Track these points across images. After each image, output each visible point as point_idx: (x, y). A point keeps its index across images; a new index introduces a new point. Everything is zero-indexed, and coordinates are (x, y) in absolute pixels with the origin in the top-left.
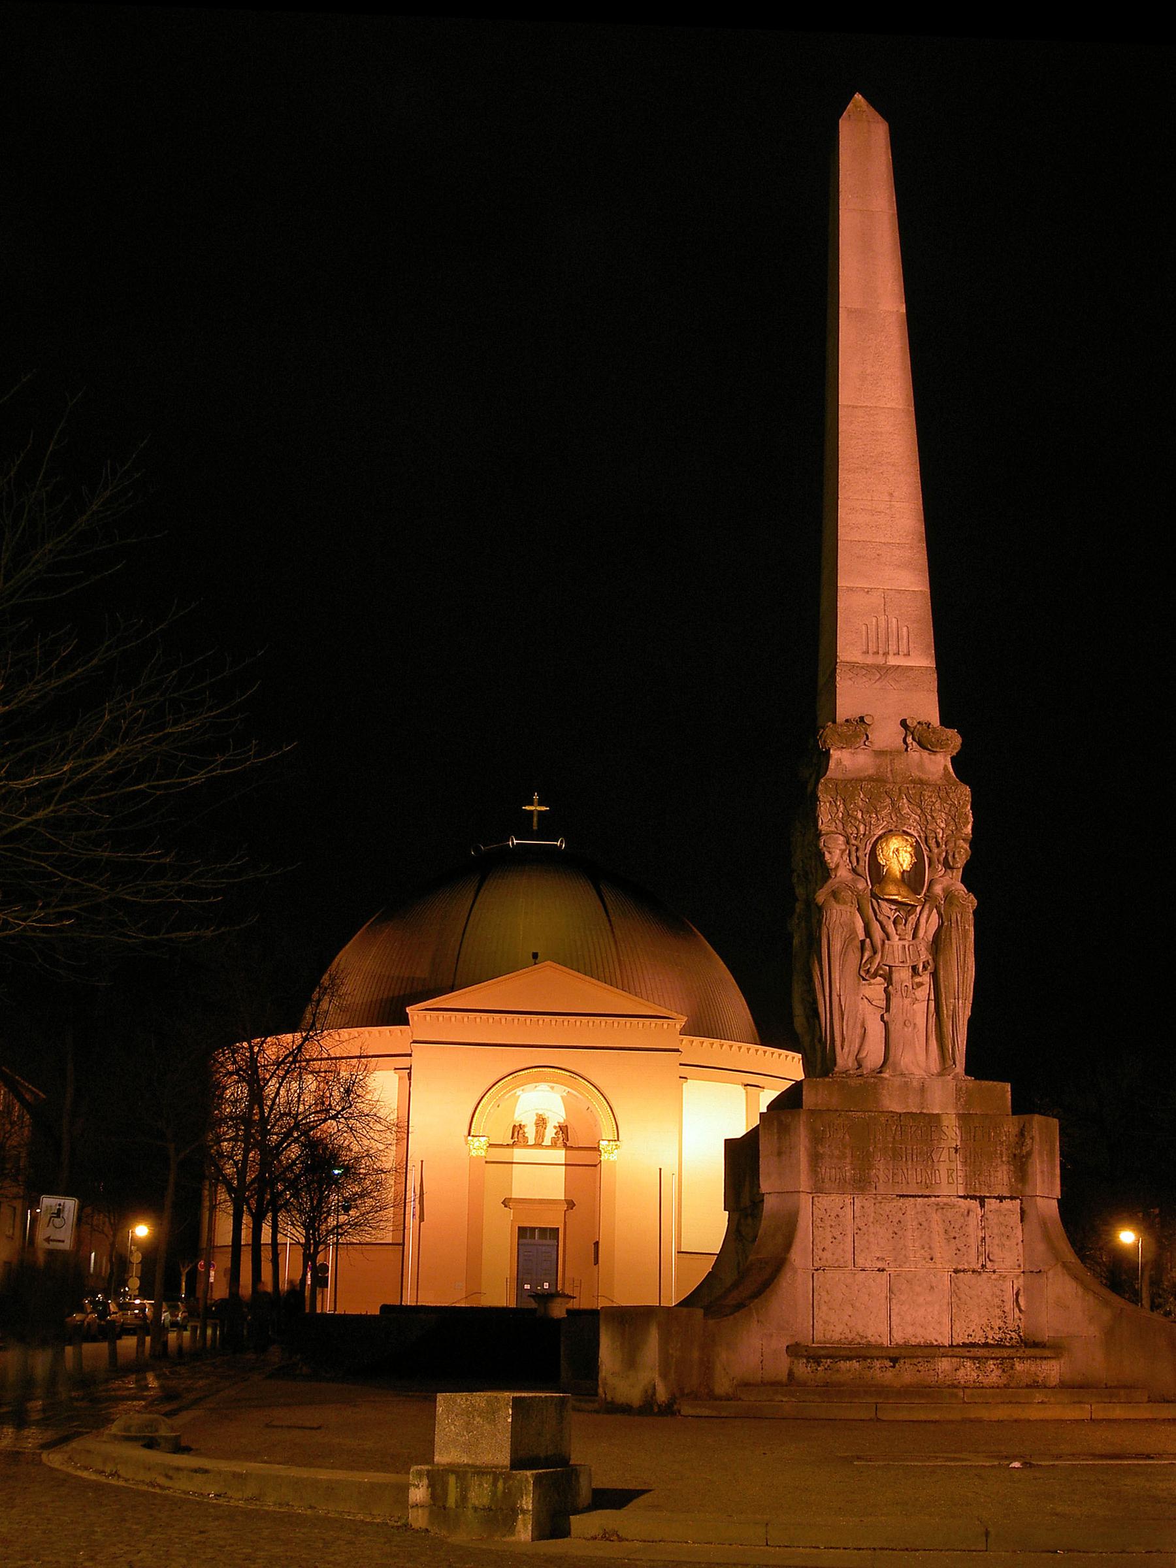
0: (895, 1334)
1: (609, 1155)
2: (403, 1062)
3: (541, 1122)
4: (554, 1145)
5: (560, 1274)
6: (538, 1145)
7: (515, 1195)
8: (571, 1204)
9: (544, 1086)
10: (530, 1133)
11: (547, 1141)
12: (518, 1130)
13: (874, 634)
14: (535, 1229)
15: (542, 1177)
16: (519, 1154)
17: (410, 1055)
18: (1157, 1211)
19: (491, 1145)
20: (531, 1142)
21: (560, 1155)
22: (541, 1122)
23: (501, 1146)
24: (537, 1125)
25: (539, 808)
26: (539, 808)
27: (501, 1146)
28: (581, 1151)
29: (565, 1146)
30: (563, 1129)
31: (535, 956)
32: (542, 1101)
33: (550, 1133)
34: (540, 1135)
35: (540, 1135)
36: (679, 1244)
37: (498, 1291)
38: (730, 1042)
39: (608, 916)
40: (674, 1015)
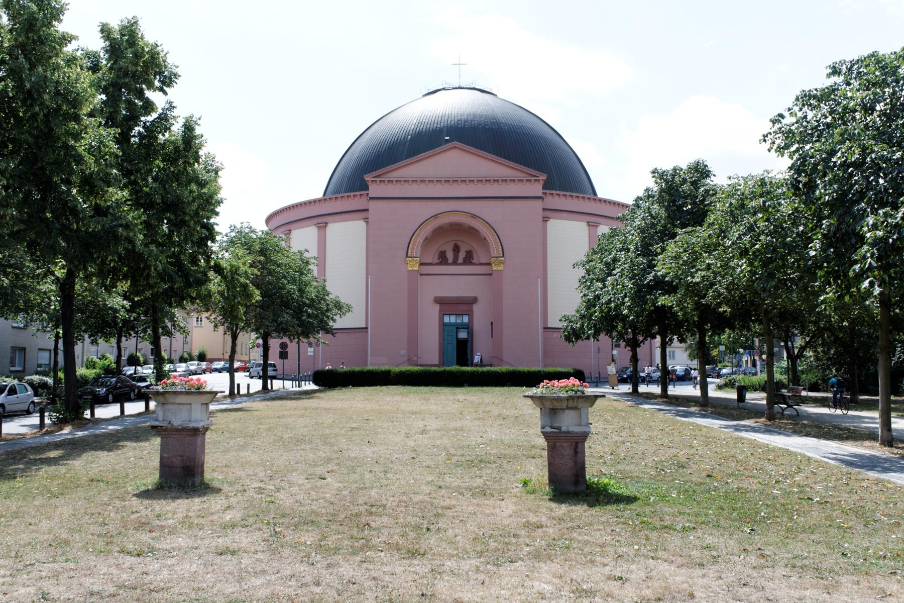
6: (455, 263)
10: (450, 256)
20: (450, 261)
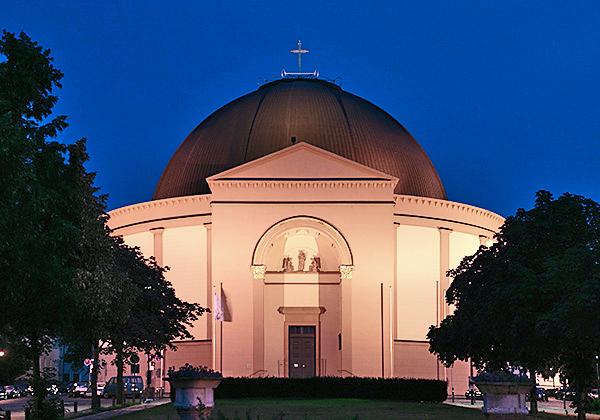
0: (517, 399)
1: (347, 275)
2: (206, 219)
3: (302, 256)
4: (311, 271)
5: (317, 357)
7: (286, 305)
8: (323, 310)
9: (303, 230)
11: (307, 269)
12: (286, 261)
13: (392, 293)
14: (298, 327)
15: (303, 294)
16: (288, 277)
17: (210, 214)
18: (556, 382)
19: (268, 272)
20: (296, 269)
21: (315, 277)
22: (302, 256)
23: (276, 272)
24: (299, 257)
25: (297, 51)
26: (297, 51)
27: (276, 272)
28: (329, 276)
29: (318, 271)
30: (317, 260)
31: (294, 140)
32: (302, 241)
33: (308, 263)
34: (302, 264)
35: (302, 264)
36: (395, 334)
37: (276, 367)
38: (430, 199)
39: (345, 114)
40: (389, 177)
